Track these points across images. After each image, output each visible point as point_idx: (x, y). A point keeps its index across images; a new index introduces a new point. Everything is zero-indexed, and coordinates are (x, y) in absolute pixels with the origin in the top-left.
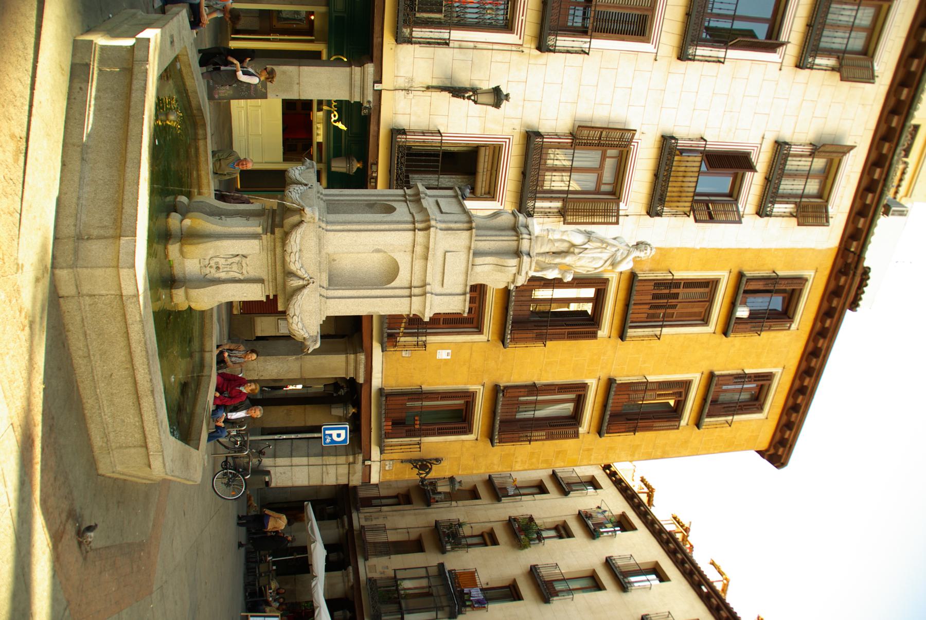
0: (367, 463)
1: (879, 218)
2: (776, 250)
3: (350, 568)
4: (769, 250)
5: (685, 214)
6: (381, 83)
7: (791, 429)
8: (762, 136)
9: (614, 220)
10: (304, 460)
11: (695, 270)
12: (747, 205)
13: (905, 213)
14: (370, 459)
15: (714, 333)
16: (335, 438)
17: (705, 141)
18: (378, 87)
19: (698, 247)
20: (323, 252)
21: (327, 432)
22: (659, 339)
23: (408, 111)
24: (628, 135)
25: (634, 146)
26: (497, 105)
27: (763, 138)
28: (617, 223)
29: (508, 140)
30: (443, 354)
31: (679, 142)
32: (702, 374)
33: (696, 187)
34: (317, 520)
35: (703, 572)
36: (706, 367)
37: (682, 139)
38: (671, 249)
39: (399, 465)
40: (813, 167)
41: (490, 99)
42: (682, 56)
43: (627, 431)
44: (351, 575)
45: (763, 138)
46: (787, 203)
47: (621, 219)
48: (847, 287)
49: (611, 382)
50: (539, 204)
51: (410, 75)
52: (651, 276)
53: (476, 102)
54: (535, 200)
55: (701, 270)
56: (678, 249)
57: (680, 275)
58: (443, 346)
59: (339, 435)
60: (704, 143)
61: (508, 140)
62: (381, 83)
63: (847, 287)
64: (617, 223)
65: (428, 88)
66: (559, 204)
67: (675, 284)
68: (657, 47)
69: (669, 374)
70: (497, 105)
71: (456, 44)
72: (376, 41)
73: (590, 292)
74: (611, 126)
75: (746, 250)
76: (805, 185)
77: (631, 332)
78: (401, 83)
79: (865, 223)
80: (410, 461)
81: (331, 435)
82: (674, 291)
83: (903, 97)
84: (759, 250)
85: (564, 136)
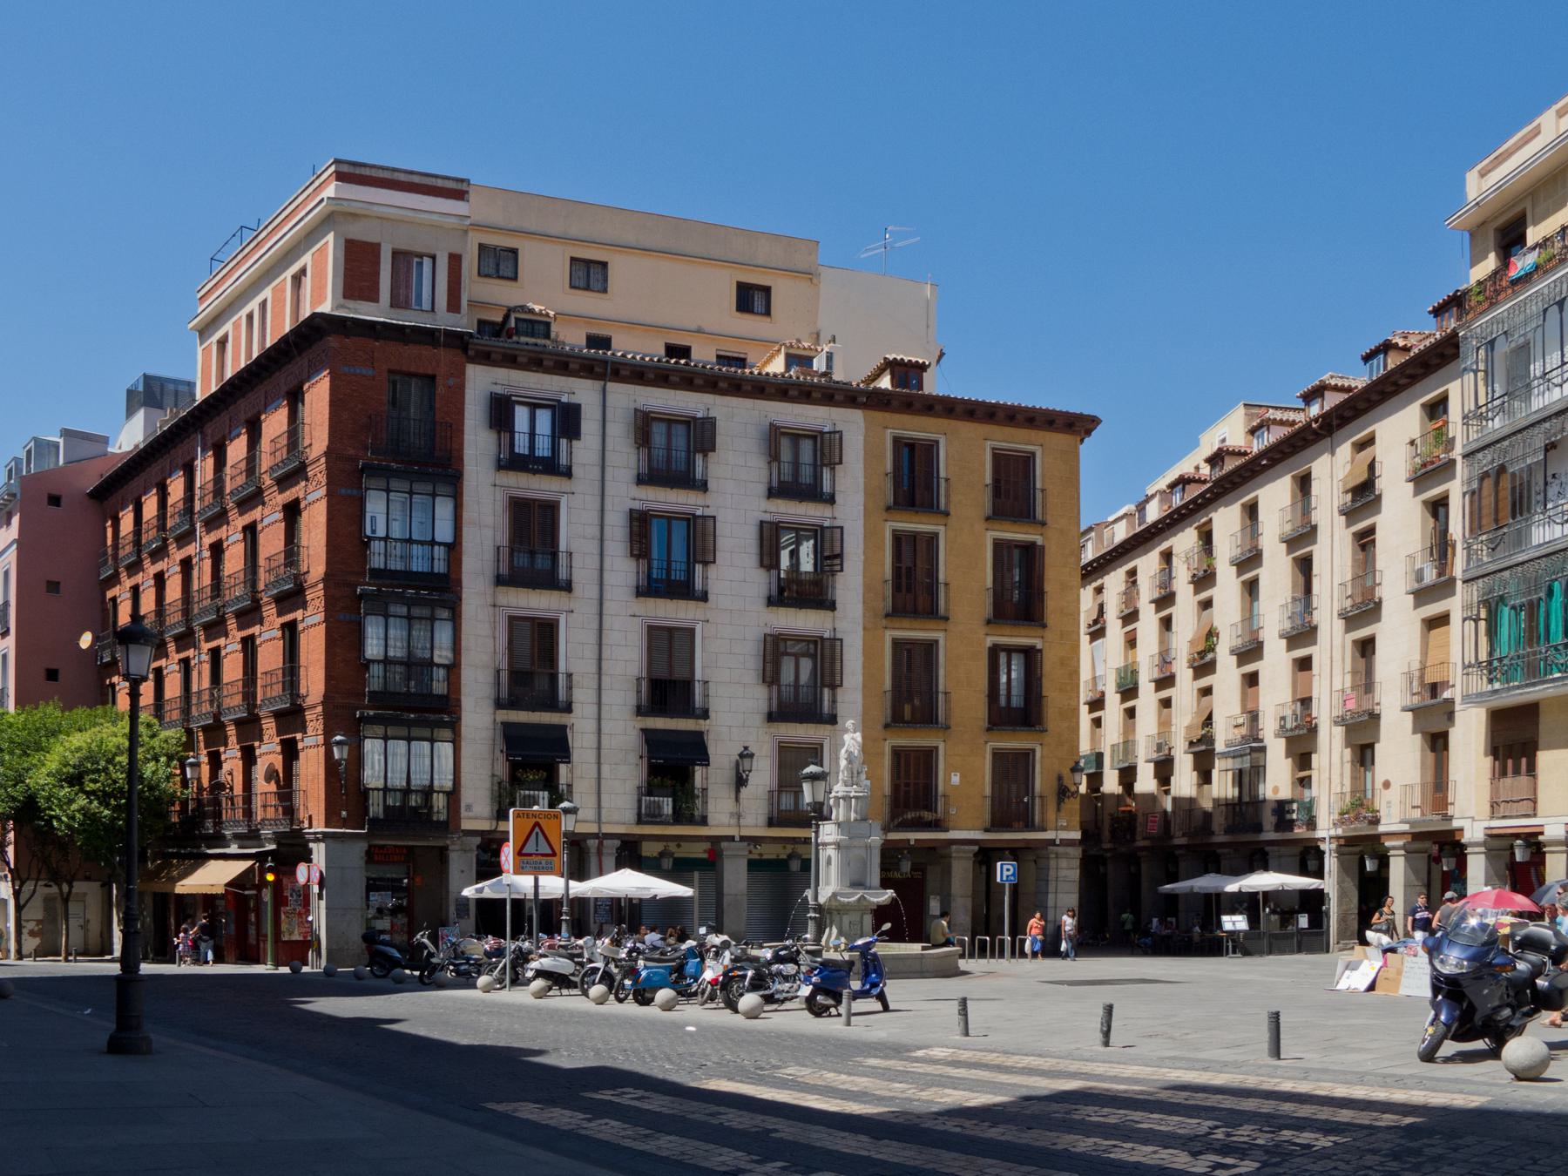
0: (1058, 842)
2: (865, 478)
3: (1219, 851)
6: (59, 583)
9: (838, 643)
10: (1051, 897)
14: (1054, 840)
16: (1011, 872)
18: (737, 839)
19: (863, 558)
21: (1005, 878)
24: (768, 638)
25: (517, 320)
26: (751, 756)
30: (956, 779)
34: (1177, 881)
35: (1183, 531)
36: (980, 526)
38: (864, 582)
39: (1062, 814)
41: (747, 762)
42: (704, 597)
43: (1042, 601)
44: (1226, 851)
46: (822, 473)
47: (838, 636)
52: (890, 600)
53: (750, 771)
56: (864, 577)
57: (888, 572)
58: (948, 779)
59: (1008, 870)
62: (59, 583)
64: (841, 640)
66: (826, 691)
67: (897, 571)
70: (751, 756)
71: (705, 781)
73: (1003, 658)
74: (762, 653)
75: (865, 509)
78: (733, 821)
80: (1059, 805)
81: (1008, 876)
82: (904, 571)
85: (770, 692)
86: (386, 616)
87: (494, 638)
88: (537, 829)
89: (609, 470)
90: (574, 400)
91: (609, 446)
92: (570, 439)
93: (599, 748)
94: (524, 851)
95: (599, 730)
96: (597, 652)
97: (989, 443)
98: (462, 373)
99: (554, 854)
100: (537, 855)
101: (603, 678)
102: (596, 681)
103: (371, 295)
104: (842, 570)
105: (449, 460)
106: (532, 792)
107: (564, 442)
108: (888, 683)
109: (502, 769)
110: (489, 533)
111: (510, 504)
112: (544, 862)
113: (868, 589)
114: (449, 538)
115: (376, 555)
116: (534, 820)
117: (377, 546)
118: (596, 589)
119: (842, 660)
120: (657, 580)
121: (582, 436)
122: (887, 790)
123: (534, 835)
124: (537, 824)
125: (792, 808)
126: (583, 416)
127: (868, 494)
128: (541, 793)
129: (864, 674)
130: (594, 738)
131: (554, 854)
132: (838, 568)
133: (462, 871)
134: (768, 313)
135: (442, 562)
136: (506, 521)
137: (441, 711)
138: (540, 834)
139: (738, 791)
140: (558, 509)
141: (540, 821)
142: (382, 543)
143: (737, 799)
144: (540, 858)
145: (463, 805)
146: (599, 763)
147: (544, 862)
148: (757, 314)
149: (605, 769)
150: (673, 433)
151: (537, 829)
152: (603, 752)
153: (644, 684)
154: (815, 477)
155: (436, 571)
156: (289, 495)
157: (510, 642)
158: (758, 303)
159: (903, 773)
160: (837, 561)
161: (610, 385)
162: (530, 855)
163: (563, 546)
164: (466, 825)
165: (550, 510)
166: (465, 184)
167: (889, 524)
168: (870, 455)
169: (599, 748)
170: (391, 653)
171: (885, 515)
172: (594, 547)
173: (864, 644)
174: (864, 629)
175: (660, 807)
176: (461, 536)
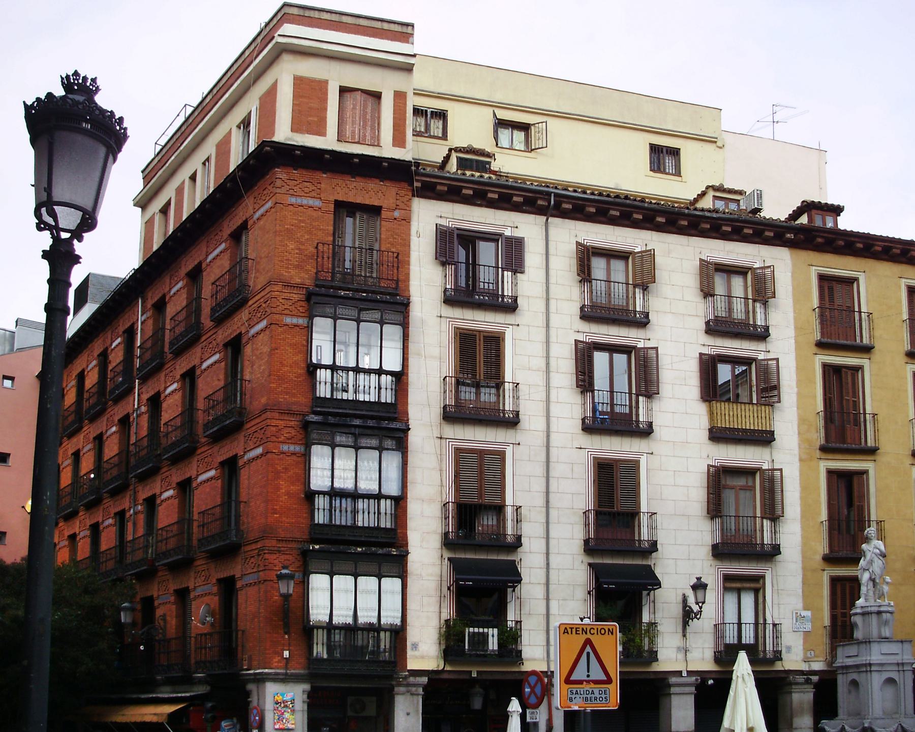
1: (765, 218)
4: (795, 319)
5: (516, 386)
7: (853, 243)
8: (702, 346)
9: (777, 473)
11: (815, 388)
12: (592, 332)
13: (759, 192)
15: (870, 359)
17: (446, 377)
18: (684, 674)
19: (796, 390)
20: (883, 717)
22: (518, 384)
23: (701, 650)
27: (704, 345)
28: (781, 470)
29: (719, 570)
31: (448, 404)
32: (907, 363)
33: (745, 403)
37: (445, 399)
38: (799, 415)
40: (605, 279)
45: (578, 332)
48: (826, 235)
49: (824, 449)
50: (509, 531)
51: (675, 650)
53: (703, 603)
54: (506, 535)
55: (815, 383)
56: (798, 408)
60: (448, 378)
61: (719, 570)
63: (826, 235)
64: (781, 470)
65: (684, 636)
68: (642, 454)
69: (907, 398)
71: (652, 616)
72: (652, 677)
76: (597, 280)
77: (870, 443)
78: (681, 656)
79: (637, 213)
83: (729, 229)
84: (796, 328)
86: (333, 446)
87: (441, 470)
88: (588, 649)
89: (553, 303)
90: (518, 234)
91: (552, 280)
92: (515, 272)
93: (547, 584)
94: (573, 678)
95: (548, 564)
96: (545, 484)
97: (904, 280)
98: (408, 209)
99: (609, 681)
100: (588, 682)
101: (551, 511)
102: (544, 515)
103: (319, 129)
104: (779, 401)
105: (396, 288)
106: (481, 630)
107: (508, 275)
108: (824, 515)
109: (448, 612)
110: (436, 364)
111: (456, 334)
112: (596, 691)
113: (802, 421)
114: (397, 368)
115: (323, 384)
116: (584, 637)
117: (323, 375)
118: (543, 421)
119: (782, 491)
120: (602, 413)
121: (526, 269)
122: (827, 622)
123: (584, 655)
124: (588, 642)
125: (736, 642)
126: (526, 250)
127: (799, 329)
128: (491, 630)
129: (801, 505)
130: (543, 572)
131: (609, 681)
132: (776, 399)
133: (408, 714)
134: (678, 173)
135: (389, 391)
136: (452, 351)
137: (392, 545)
138: (592, 655)
139: (685, 624)
140: (504, 340)
141: (592, 638)
142: (329, 371)
143: (684, 636)
144: (592, 685)
145: (409, 644)
146: (548, 599)
147: (596, 691)
148: (668, 174)
149: (554, 604)
150: (612, 268)
151: (588, 649)
152: (551, 587)
153: (592, 516)
154: (747, 312)
155: (383, 401)
156: (225, 333)
157: (457, 475)
158: (669, 162)
159: (839, 602)
160: (776, 393)
161: (551, 219)
162: (580, 682)
163: (508, 377)
164: (412, 665)
165: (495, 342)
166: (410, 28)
167: (819, 357)
168: (799, 295)
169: (547, 584)
170: (337, 485)
171: (815, 350)
172: (540, 379)
173: (801, 475)
174: (801, 460)
175: (485, 637)
176: (408, 366)
